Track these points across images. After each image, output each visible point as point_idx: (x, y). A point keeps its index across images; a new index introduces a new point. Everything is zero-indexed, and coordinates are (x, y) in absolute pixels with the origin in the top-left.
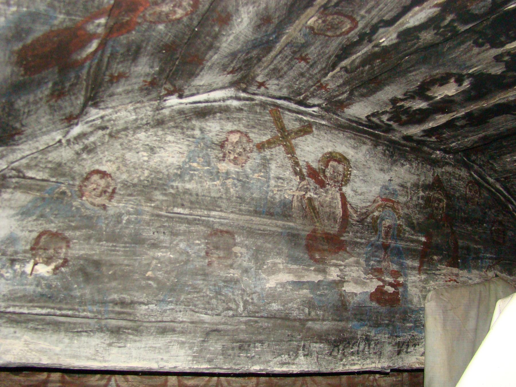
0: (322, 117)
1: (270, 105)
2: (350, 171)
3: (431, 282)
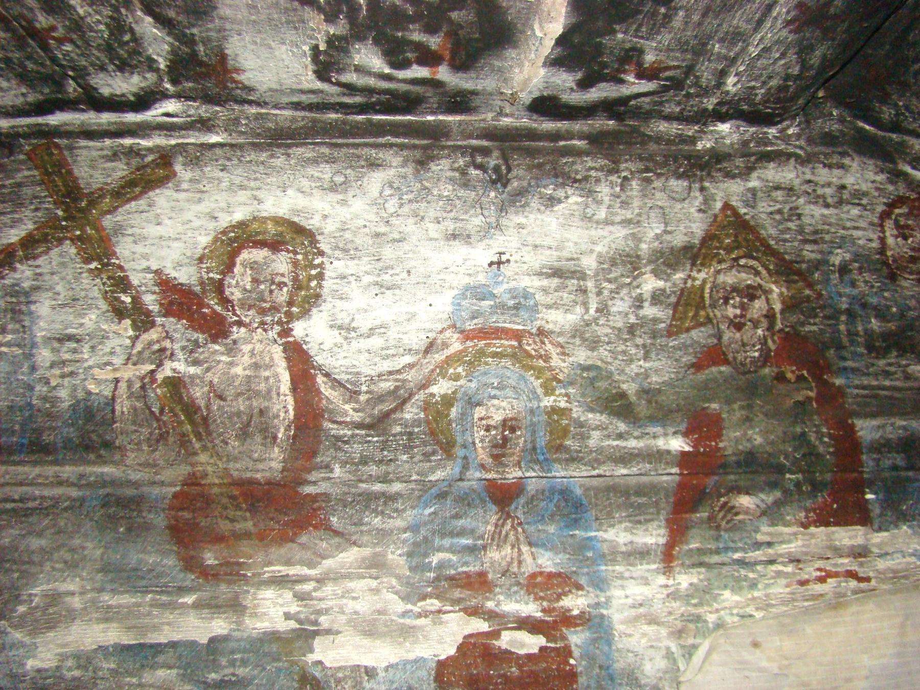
0: (205, 125)
1: (27, 136)
2: (320, 265)
3: (727, 594)
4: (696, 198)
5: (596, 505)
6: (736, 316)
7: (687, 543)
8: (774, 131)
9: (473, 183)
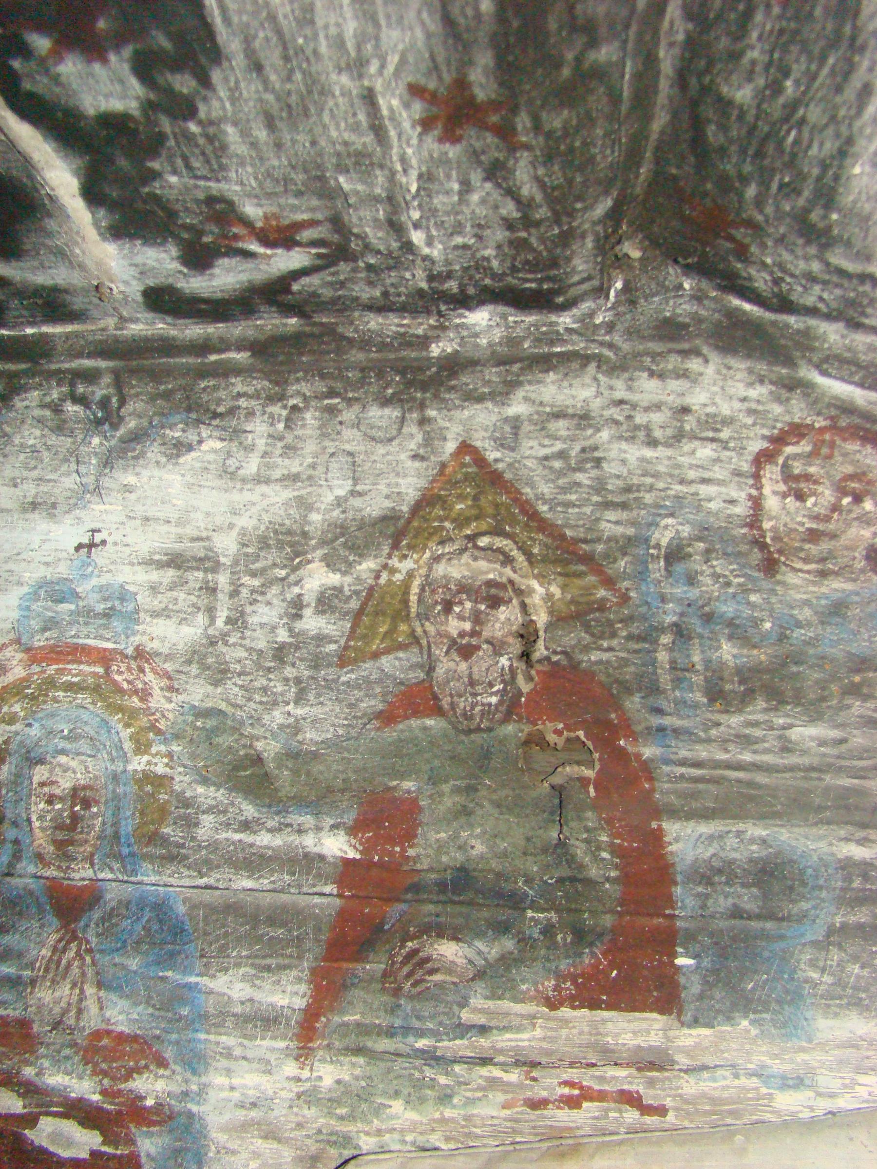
3: (397, 1106)
4: (412, 436)
5: (206, 934)
6: (462, 634)
7: (342, 1012)
8: (568, 320)
9: (71, 425)
